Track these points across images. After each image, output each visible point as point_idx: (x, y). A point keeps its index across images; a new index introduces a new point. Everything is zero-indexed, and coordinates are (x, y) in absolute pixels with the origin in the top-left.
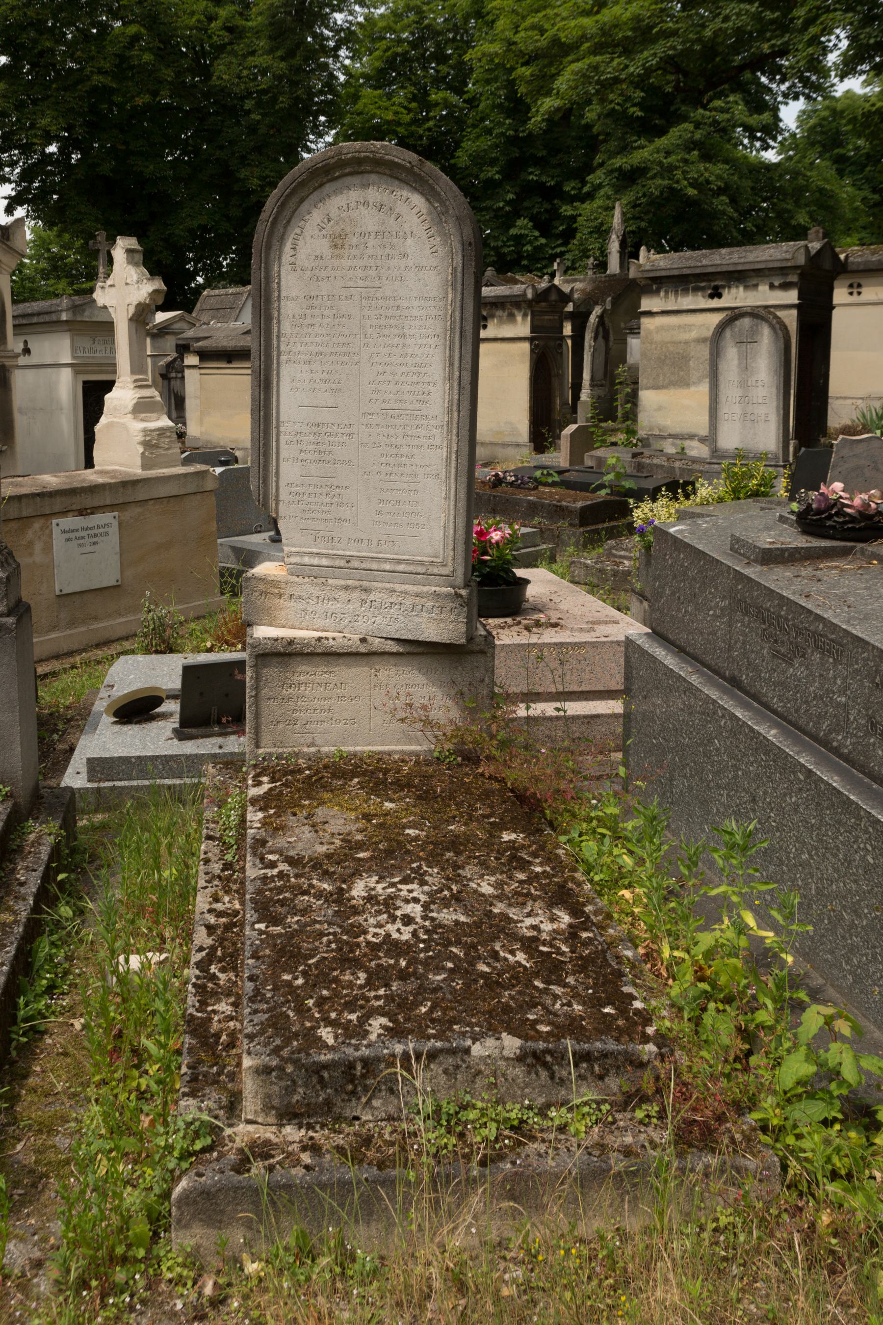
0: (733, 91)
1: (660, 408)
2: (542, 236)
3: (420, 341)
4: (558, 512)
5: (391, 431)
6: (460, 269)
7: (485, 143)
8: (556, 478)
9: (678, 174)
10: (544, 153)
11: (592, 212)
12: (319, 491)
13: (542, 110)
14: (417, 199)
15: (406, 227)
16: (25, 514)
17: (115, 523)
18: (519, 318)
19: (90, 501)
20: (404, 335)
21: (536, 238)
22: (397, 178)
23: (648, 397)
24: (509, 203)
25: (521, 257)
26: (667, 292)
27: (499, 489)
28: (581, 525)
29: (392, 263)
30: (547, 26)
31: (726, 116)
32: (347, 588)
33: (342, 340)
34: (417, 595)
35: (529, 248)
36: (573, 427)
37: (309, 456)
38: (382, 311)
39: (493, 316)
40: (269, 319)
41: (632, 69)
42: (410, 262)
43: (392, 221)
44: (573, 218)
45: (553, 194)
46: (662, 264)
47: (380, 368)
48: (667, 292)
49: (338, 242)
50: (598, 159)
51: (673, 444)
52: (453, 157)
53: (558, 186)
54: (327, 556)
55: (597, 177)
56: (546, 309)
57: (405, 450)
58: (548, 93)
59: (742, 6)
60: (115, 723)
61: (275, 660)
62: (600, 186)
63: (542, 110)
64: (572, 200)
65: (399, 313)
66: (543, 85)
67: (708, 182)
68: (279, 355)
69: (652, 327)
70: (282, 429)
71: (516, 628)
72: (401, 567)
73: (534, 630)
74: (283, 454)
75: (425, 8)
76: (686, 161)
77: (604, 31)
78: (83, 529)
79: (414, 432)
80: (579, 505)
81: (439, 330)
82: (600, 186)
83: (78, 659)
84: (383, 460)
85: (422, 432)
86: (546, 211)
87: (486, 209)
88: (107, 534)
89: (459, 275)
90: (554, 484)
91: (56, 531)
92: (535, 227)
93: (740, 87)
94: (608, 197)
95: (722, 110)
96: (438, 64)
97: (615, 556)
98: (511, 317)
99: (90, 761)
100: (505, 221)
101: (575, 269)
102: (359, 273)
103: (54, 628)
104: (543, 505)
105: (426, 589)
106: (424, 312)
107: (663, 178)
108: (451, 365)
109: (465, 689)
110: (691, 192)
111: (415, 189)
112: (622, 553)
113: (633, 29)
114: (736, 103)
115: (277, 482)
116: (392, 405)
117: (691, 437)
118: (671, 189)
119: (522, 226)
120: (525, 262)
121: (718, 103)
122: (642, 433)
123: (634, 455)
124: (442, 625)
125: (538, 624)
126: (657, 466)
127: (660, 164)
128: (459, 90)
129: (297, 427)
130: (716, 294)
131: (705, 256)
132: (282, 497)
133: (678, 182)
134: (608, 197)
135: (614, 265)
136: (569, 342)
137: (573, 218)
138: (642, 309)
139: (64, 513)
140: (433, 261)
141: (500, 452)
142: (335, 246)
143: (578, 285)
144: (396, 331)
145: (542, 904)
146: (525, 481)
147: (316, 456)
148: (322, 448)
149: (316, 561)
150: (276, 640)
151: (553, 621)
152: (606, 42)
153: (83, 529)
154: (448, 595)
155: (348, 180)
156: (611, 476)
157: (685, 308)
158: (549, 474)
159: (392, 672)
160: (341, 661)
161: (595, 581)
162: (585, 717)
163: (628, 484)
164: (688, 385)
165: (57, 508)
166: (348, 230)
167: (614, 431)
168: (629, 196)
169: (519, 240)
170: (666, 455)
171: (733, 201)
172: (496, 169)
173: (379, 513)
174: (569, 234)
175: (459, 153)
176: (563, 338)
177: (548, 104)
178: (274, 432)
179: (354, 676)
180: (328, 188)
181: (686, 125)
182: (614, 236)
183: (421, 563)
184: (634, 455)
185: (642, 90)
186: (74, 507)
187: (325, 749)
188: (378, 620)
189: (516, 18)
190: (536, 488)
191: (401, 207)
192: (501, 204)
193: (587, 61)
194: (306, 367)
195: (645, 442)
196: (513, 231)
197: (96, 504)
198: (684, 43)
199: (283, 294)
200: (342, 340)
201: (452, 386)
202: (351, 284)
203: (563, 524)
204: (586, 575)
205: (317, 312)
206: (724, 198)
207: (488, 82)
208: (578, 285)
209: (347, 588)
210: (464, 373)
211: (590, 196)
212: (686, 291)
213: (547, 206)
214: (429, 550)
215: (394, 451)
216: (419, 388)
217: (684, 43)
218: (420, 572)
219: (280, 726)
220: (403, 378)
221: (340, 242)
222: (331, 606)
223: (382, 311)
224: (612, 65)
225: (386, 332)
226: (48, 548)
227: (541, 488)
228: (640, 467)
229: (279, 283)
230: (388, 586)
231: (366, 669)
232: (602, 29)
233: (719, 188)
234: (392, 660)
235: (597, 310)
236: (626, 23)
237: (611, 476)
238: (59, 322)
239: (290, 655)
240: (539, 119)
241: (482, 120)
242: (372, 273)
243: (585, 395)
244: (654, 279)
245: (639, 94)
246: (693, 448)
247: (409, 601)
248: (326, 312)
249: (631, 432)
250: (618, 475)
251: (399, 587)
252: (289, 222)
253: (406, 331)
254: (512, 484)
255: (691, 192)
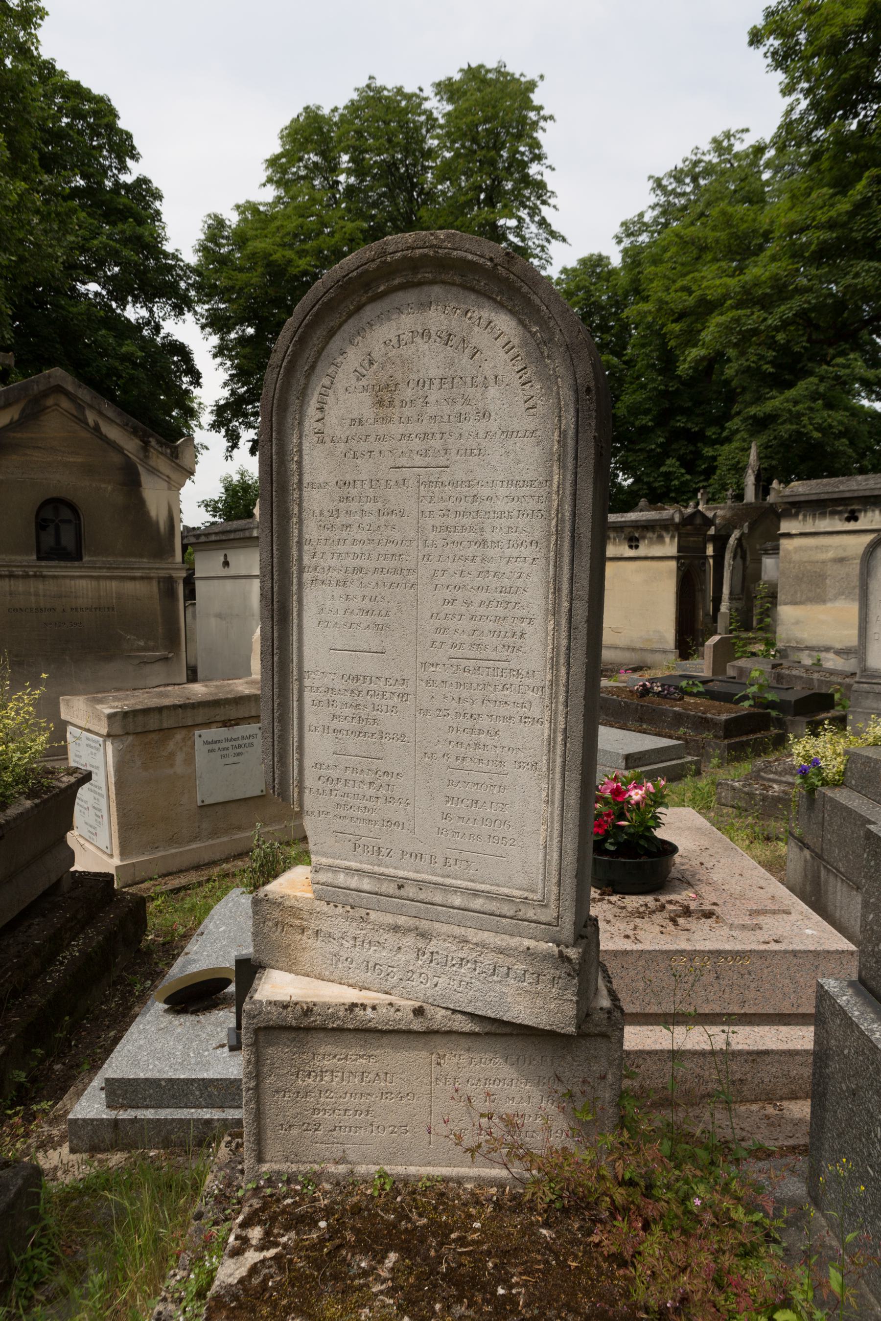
0: (853, 350)
1: (797, 622)
2: (687, 473)
3: (508, 552)
4: (703, 723)
5: (465, 693)
6: (571, 433)
7: (640, 396)
8: (701, 688)
9: (805, 420)
10: (690, 404)
11: (730, 453)
12: (359, 777)
13: (689, 359)
14: (505, 323)
15: (488, 369)
16: (165, 725)
17: (259, 733)
18: (667, 540)
19: (234, 713)
20: (484, 542)
21: (683, 475)
22: (473, 290)
23: (786, 612)
24: (658, 446)
25: (668, 490)
26: (805, 516)
27: (646, 698)
28: (726, 737)
29: (466, 426)
30: (694, 288)
31: (848, 371)
32: (396, 929)
33: (391, 549)
34: (500, 951)
35: (676, 482)
36: (716, 638)
37: (344, 725)
38: (450, 504)
39: (644, 538)
40: (285, 517)
41: (770, 322)
42: (493, 426)
43: (465, 359)
44: (714, 458)
45: (698, 437)
46: (801, 490)
47: (448, 594)
48: (805, 516)
49: (384, 397)
50: (736, 408)
51: (810, 656)
52: (614, 407)
53: (702, 432)
54: (371, 875)
55: (734, 424)
56: (691, 531)
57: (485, 723)
58: (695, 345)
59: (871, 264)
60: (166, 1011)
61: (285, 1035)
62: (737, 431)
63: (689, 359)
64: (713, 443)
65: (475, 506)
66: (690, 338)
67: (831, 426)
68: (301, 571)
69: (790, 548)
70: (307, 682)
71: (658, 918)
72: (478, 903)
73: (681, 921)
74: (310, 719)
75: (592, 288)
76: (811, 409)
77: (746, 290)
78: (227, 740)
79: (500, 695)
80: (724, 717)
81: (538, 535)
82: (737, 431)
83: (216, 870)
84: (452, 736)
85: (512, 696)
86: (691, 452)
87: (641, 450)
88: (251, 745)
89: (570, 442)
90: (698, 695)
91: (198, 743)
92: (681, 466)
93: (857, 347)
94: (744, 440)
95: (844, 366)
96: (602, 333)
97: (764, 779)
98: (661, 539)
99: (107, 1080)
100: (656, 460)
101: (714, 500)
102: (416, 444)
103: (194, 839)
104: (688, 716)
105: (514, 942)
106: (514, 505)
107: (792, 424)
108: (557, 590)
109: (576, 1090)
110: (816, 435)
111: (501, 305)
112: (771, 776)
113: (772, 287)
114: (856, 359)
115: (301, 761)
116: (466, 652)
117: (827, 649)
118: (798, 432)
119: (671, 464)
120: (673, 495)
121: (840, 360)
122: (780, 645)
123: (774, 666)
124: (539, 1002)
125: (687, 912)
126: (796, 677)
127: (790, 411)
128: (619, 355)
129: (327, 680)
130: (853, 517)
131: (842, 483)
132: (308, 783)
133: (804, 427)
134: (744, 440)
135: (750, 495)
136: (711, 561)
137: (714, 458)
138: (782, 531)
139: (208, 724)
140: (529, 423)
141: (650, 658)
142: (381, 403)
143: (720, 512)
144: (472, 536)
145: (657, 254)
146: (673, 689)
147: (355, 725)
148: (363, 714)
149: (354, 882)
150: (285, 1006)
151: (707, 907)
152: (748, 298)
153: (227, 740)
154: (546, 957)
155: (400, 297)
156: (754, 689)
157: (822, 530)
158: (694, 684)
159: (464, 1059)
160: (385, 1040)
161: (742, 804)
162: (750, 1053)
163: (770, 696)
164: (824, 601)
165: (199, 720)
166: (399, 376)
167: (754, 641)
168: (764, 438)
169: (668, 476)
170: (804, 666)
171: (852, 443)
172: (649, 417)
173: (446, 816)
174: (711, 471)
175: (619, 404)
176: (706, 558)
177: (694, 353)
178: (296, 687)
179: (406, 1063)
180: (369, 312)
181: (812, 379)
182: (750, 471)
183: (509, 899)
184: (774, 666)
185: (774, 350)
186: (218, 718)
187: (361, 1169)
188: (442, 981)
189: (666, 282)
190: (681, 699)
191: (479, 337)
192: (653, 447)
193: (731, 314)
194: (340, 591)
195: (783, 653)
196: (663, 469)
197: (241, 715)
198: (817, 297)
199: (307, 479)
200: (391, 549)
201: (557, 624)
202: (404, 461)
203: (708, 735)
204: (734, 798)
205: (354, 506)
206: (844, 441)
207: (643, 346)
208: (720, 512)
209: (396, 929)
210: (577, 604)
211: (728, 440)
212: (823, 515)
213: (692, 448)
214: (520, 879)
215: (468, 723)
216: (506, 627)
217: (817, 297)
218: (508, 915)
219: (295, 1132)
220: (482, 610)
221: (386, 396)
222: (374, 954)
223: (450, 504)
224: (753, 318)
225: (456, 537)
226: (190, 760)
227: (687, 699)
228: (779, 678)
229: (300, 463)
230: (458, 931)
231: (424, 1054)
232: (743, 287)
233: (840, 432)
234: (464, 1042)
235: (736, 534)
236: (765, 282)
237: (754, 689)
238: (251, 538)
239: (308, 1029)
240: (686, 366)
241: (638, 378)
242: (436, 443)
243: (724, 608)
244: (794, 504)
245: (771, 354)
246: (828, 660)
247: (488, 959)
248: (366, 507)
249: (770, 643)
250: (761, 686)
251: (476, 936)
252: (313, 367)
253: (488, 536)
254: (658, 694)
255: (816, 435)
